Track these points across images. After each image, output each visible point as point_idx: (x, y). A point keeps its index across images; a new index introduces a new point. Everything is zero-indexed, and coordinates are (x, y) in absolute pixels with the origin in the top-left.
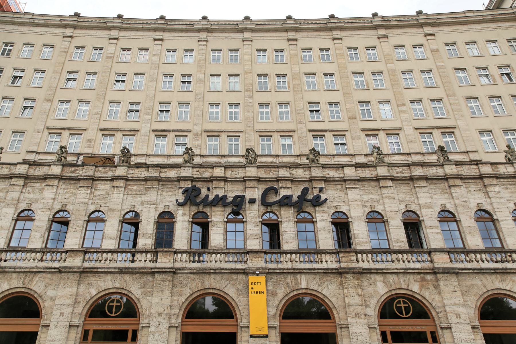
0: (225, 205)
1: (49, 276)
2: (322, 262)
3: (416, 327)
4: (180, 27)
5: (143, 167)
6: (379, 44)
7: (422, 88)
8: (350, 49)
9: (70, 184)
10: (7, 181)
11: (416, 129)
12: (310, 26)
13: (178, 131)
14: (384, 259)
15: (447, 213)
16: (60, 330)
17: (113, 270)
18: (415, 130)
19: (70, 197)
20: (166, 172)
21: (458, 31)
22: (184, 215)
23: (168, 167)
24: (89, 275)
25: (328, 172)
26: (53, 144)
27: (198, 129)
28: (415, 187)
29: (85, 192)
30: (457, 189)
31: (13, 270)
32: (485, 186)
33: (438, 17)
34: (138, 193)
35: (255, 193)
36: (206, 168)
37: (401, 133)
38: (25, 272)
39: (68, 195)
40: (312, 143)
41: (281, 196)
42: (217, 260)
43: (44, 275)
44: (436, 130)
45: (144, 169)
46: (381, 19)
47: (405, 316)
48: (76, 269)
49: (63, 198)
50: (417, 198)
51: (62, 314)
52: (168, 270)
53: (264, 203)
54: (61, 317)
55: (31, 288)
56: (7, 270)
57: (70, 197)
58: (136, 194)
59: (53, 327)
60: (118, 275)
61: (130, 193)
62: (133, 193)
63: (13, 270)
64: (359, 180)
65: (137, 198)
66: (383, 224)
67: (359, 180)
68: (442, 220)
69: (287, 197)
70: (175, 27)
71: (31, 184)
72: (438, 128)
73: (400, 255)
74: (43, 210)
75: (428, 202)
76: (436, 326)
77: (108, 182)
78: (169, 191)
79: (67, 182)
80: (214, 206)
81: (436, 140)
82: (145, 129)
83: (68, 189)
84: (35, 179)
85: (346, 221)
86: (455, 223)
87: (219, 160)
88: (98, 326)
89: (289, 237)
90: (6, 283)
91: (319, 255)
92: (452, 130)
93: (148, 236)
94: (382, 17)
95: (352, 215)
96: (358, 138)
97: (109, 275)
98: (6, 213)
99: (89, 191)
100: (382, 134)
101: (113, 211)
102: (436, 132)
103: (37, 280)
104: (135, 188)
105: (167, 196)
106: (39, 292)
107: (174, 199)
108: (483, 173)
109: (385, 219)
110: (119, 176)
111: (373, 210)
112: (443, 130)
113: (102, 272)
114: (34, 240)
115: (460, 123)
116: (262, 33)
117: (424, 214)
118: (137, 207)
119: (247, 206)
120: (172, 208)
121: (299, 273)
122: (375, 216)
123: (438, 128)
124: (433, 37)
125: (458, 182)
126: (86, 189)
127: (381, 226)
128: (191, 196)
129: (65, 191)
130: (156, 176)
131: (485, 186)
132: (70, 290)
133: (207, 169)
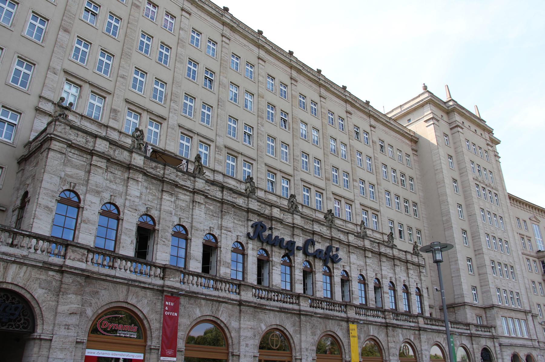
0: (281, 247)
1: (230, 306)
2: (126, 270)
3: (270, 357)
4: (210, 10)
5: (217, 186)
6: (179, 16)
7: (200, 86)
8: (194, 30)
9: (152, 183)
10: (85, 156)
11: (179, 126)
12: (309, 74)
13: (203, 137)
14: (152, 273)
15: (113, 207)
16: (248, 359)
17: (274, 309)
18: (125, 103)
19: (154, 199)
20: (236, 198)
21: (386, 133)
22: (253, 249)
23: (238, 194)
24: (259, 310)
25: (339, 235)
26: (129, 122)
27: (221, 142)
28: (91, 164)
29: (170, 199)
30: (135, 183)
31: (204, 297)
32: (349, 252)
33: (381, 116)
34: (214, 215)
35: (299, 242)
36: (266, 205)
37: (165, 124)
38: (213, 300)
39: (151, 197)
40: (332, 205)
41: (316, 249)
42: (126, 268)
43: (226, 305)
44: (88, 85)
45: (218, 189)
46: (230, 18)
47: (275, 348)
48: (253, 304)
49: (147, 199)
50: (381, 270)
51: (247, 345)
52: (215, 299)
53: (306, 253)
54: (247, 348)
55: (219, 317)
56: (200, 296)
57: (154, 199)
58: (213, 216)
59: (243, 357)
60: (277, 313)
61: (208, 212)
62: (211, 213)
63: (204, 297)
64: (356, 247)
65: (214, 220)
66: (77, 209)
67: (356, 247)
68: (104, 213)
69: (320, 251)
70: (205, 7)
71: (112, 170)
72: (91, 85)
73: (34, 241)
74: (130, 210)
75: (169, 210)
76: (292, 357)
77: (188, 194)
78: (240, 220)
79: (150, 179)
80: (275, 246)
81: (105, 108)
82: (174, 120)
83: (150, 189)
84: (116, 164)
85: (151, 228)
86: (116, 221)
87: (238, 185)
88: (267, 357)
89: (277, 277)
90: (198, 310)
91: (124, 261)
92: (104, 94)
93: (227, 265)
94: (231, 16)
95: (352, 275)
96: (330, 199)
97: (271, 312)
98: (92, 203)
99: (173, 200)
100: (145, 116)
101: (197, 230)
102: (145, 115)
103: (222, 309)
104: (211, 208)
105: (238, 226)
106: (225, 322)
107: (245, 232)
108: (133, 163)
109: (121, 216)
110: (202, 191)
111: (149, 213)
112: (270, 169)
113: (270, 310)
114: (125, 245)
115: (382, 209)
116: (273, 59)
117: (384, 282)
118: (215, 230)
119: (295, 252)
120: (243, 240)
121: (370, 324)
122: (111, 209)
123: (91, 85)
124: (187, 16)
125: (140, 177)
126: (170, 196)
127: (113, 223)
128: (258, 233)
129: (148, 191)
130: (223, 198)
131: (394, 265)
132: (249, 323)
133: (267, 206)
